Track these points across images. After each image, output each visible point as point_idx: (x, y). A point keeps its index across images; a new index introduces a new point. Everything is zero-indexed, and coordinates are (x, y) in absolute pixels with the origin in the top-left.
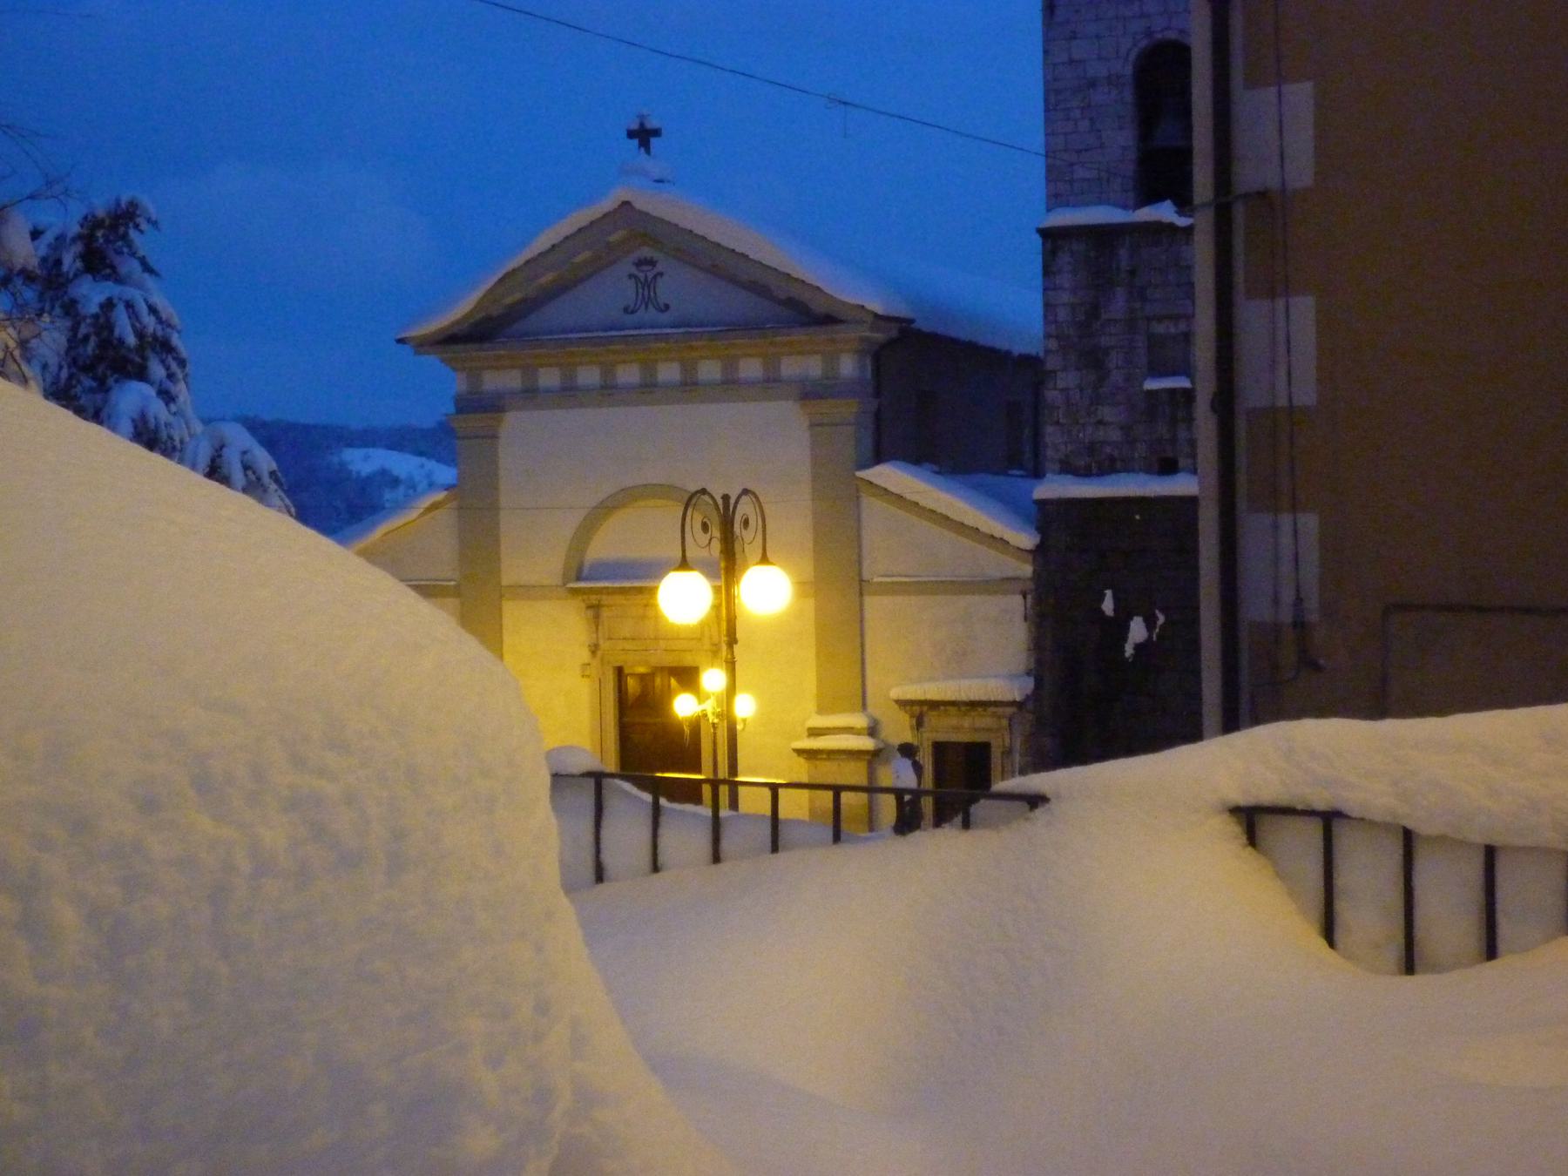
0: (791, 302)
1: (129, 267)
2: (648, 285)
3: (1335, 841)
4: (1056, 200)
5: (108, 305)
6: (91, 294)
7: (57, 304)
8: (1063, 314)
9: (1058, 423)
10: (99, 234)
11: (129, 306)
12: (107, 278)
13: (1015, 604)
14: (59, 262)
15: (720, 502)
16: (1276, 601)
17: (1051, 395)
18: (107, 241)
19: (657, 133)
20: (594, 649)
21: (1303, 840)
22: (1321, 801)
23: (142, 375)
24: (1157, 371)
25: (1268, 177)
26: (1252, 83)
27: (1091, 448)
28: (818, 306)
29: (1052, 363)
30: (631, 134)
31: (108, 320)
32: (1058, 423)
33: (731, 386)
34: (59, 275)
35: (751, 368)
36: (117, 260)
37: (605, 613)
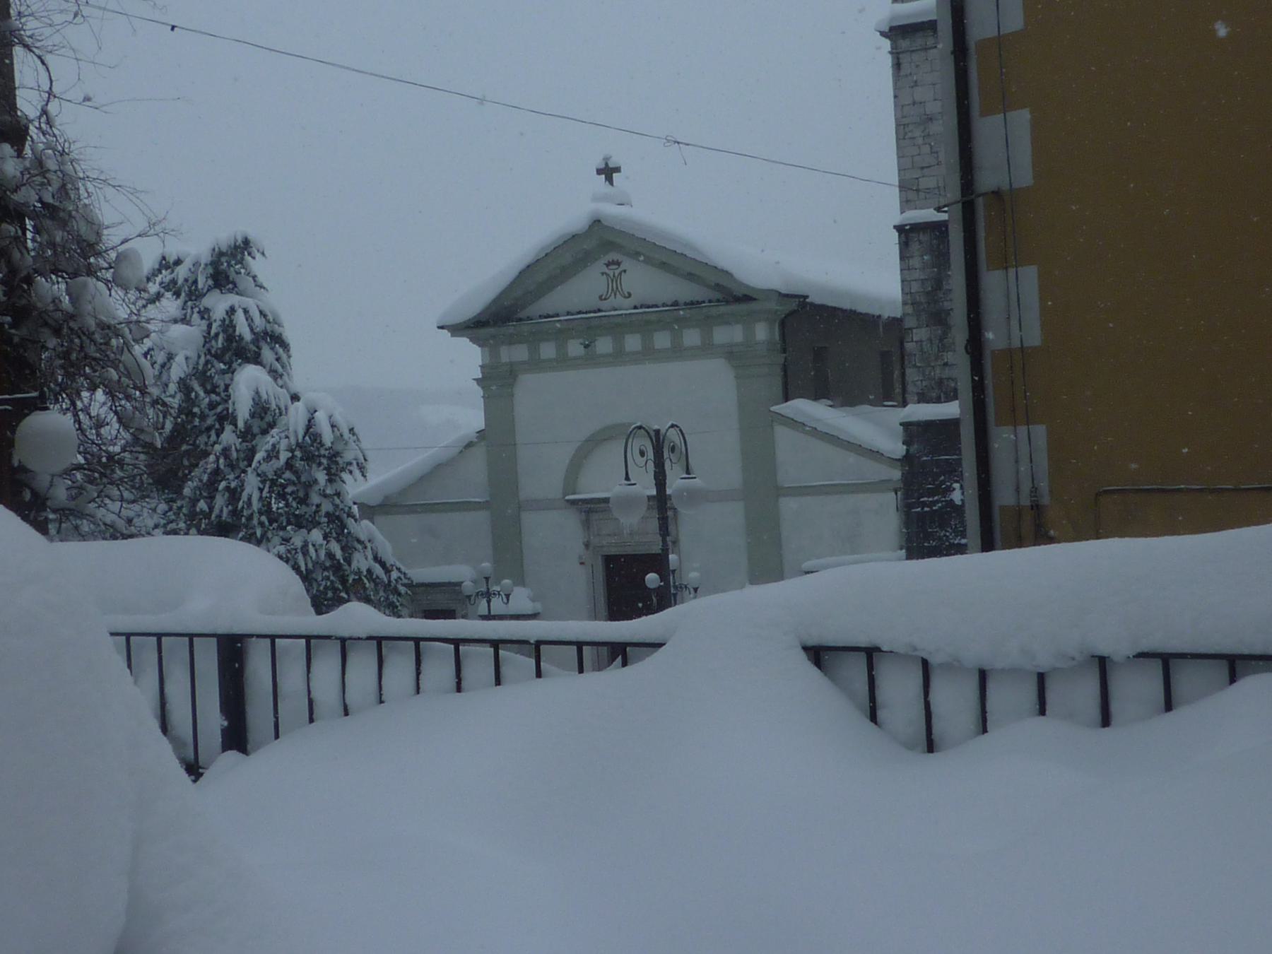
0: (718, 287)
1: (245, 283)
2: (616, 279)
3: (1211, 661)
4: (906, 204)
5: (232, 311)
6: (219, 303)
7: (196, 310)
8: (915, 287)
9: (915, 366)
10: (224, 259)
11: (246, 311)
12: (230, 291)
14: (195, 282)
15: (653, 434)
16: (1018, 490)
17: (909, 346)
18: (229, 265)
19: (618, 170)
21: (856, 669)
22: (863, 640)
23: (256, 360)
26: (985, 113)
27: (940, 382)
28: (739, 292)
29: (910, 322)
30: (599, 172)
31: (231, 321)
32: (915, 366)
33: (678, 352)
34: (197, 289)
35: (692, 337)
36: (238, 279)
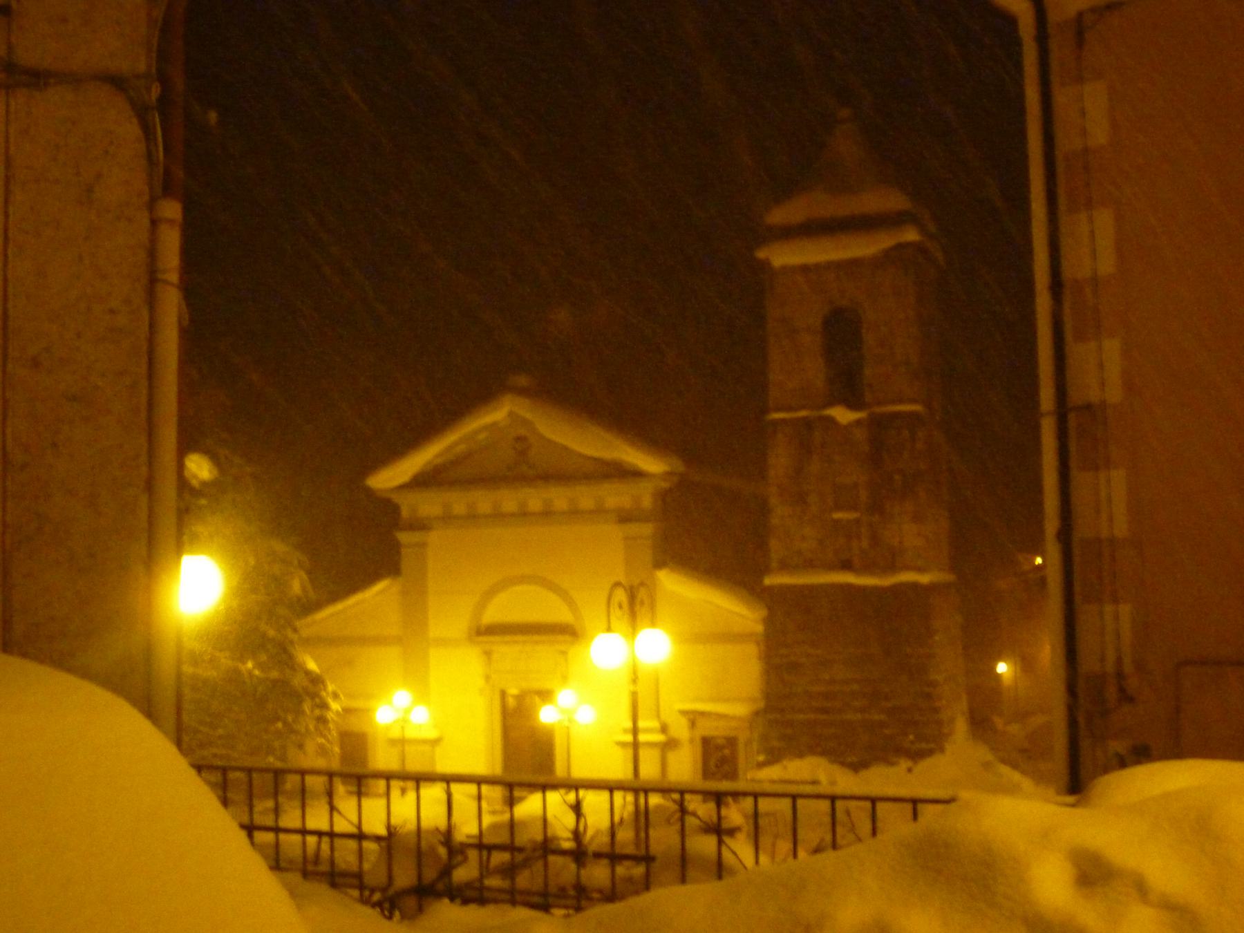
13: (752, 650)
20: (487, 678)
24: (838, 507)
25: (1094, 396)
37: (495, 656)
